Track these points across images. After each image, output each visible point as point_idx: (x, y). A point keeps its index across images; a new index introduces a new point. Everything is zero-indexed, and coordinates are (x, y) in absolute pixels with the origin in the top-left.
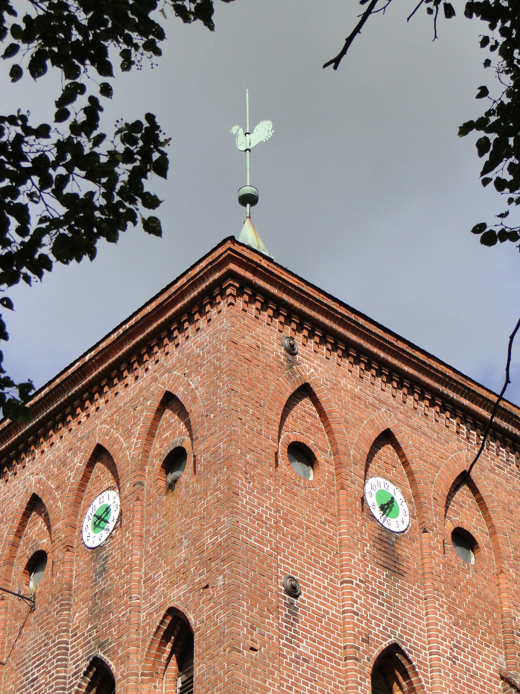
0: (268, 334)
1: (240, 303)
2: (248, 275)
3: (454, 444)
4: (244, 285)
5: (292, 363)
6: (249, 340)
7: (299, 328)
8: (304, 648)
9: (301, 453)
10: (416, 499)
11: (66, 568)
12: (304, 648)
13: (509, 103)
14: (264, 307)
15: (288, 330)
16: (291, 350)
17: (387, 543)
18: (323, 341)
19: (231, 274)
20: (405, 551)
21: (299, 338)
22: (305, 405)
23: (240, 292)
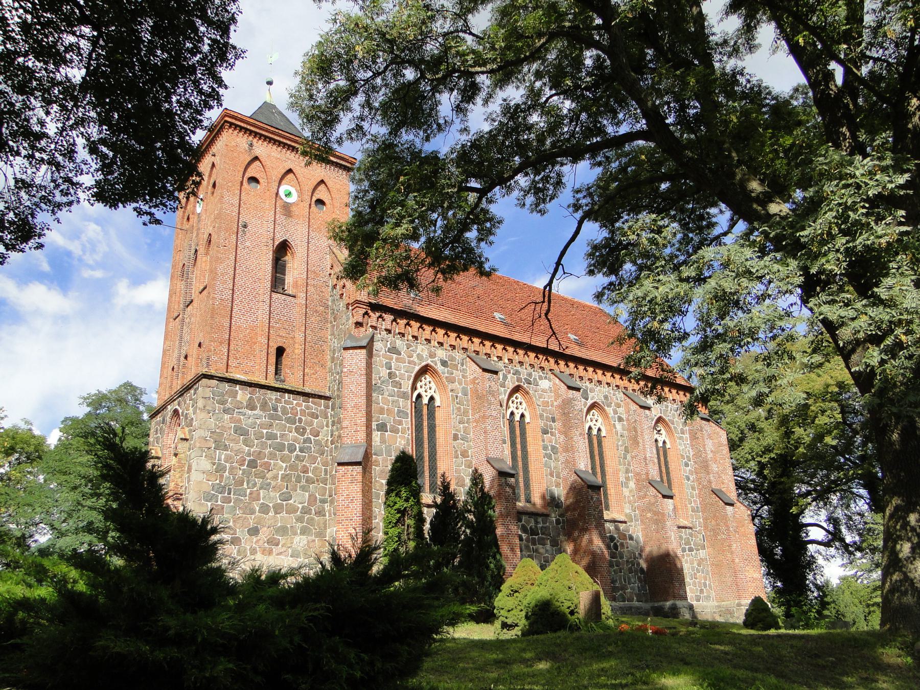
0: (241, 141)
1: (230, 131)
2: (233, 121)
3: (319, 170)
4: (231, 124)
5: (250, 150)
6: (233, 144)
7: (255, 137)
8: (248, 244)
9: (254, 180)
10: (300, 192)
11: (194, 219)
12: (248, 244)
13: (416, 321)
14: (245, 133)
15: (251, 138)
16: (251, 145)
17: (287, 208)
18: (274, 144)
19: (226, 121)
20: (294, 209)
21: (255, 140)
22: (257, 163)
23: (230, 127)
